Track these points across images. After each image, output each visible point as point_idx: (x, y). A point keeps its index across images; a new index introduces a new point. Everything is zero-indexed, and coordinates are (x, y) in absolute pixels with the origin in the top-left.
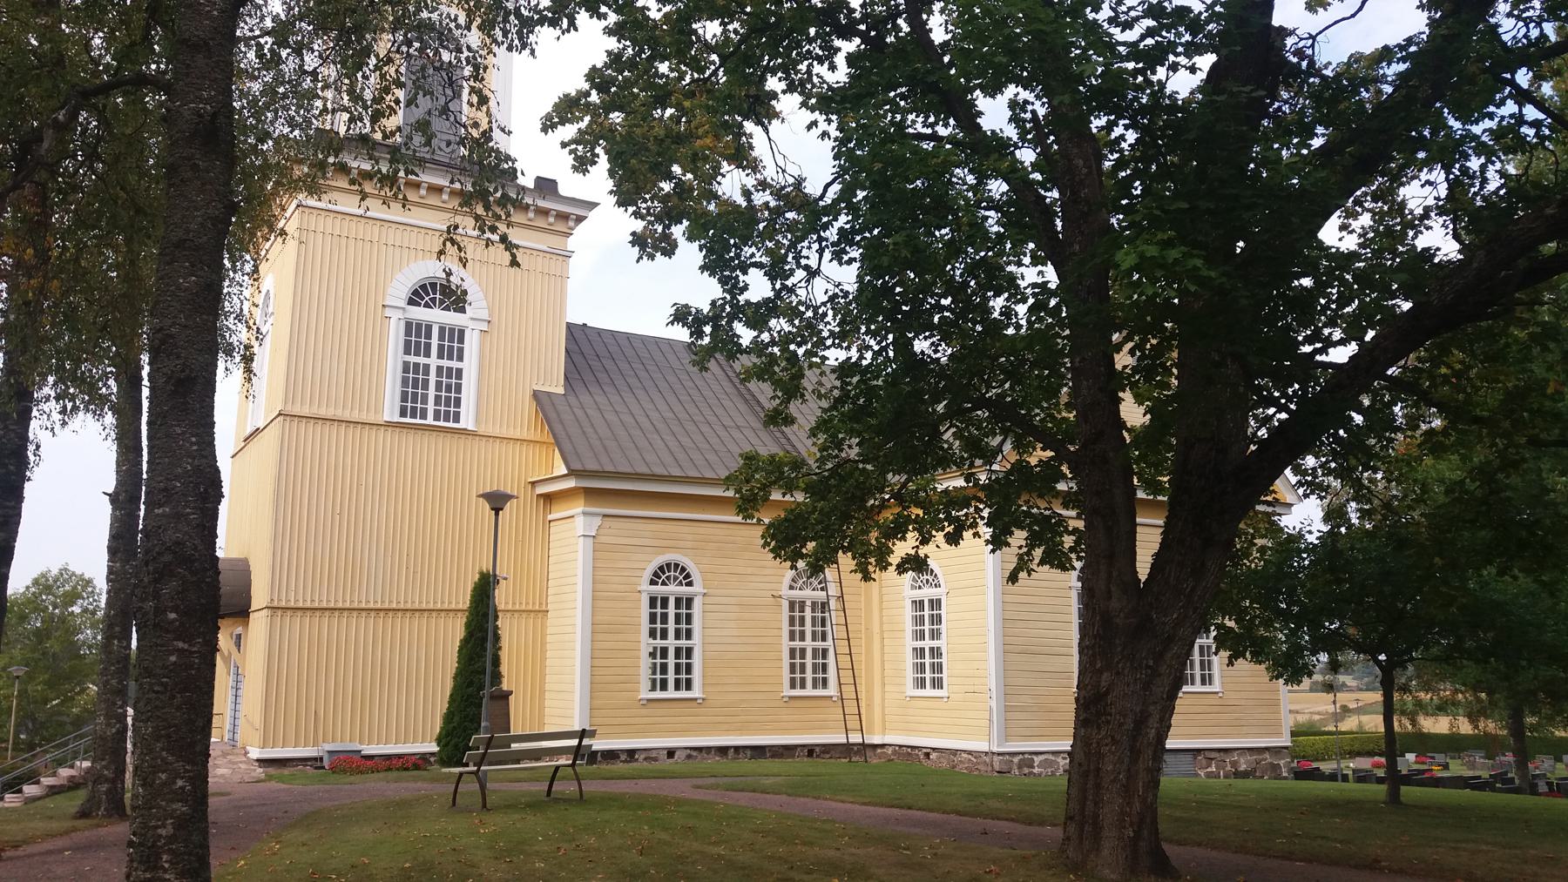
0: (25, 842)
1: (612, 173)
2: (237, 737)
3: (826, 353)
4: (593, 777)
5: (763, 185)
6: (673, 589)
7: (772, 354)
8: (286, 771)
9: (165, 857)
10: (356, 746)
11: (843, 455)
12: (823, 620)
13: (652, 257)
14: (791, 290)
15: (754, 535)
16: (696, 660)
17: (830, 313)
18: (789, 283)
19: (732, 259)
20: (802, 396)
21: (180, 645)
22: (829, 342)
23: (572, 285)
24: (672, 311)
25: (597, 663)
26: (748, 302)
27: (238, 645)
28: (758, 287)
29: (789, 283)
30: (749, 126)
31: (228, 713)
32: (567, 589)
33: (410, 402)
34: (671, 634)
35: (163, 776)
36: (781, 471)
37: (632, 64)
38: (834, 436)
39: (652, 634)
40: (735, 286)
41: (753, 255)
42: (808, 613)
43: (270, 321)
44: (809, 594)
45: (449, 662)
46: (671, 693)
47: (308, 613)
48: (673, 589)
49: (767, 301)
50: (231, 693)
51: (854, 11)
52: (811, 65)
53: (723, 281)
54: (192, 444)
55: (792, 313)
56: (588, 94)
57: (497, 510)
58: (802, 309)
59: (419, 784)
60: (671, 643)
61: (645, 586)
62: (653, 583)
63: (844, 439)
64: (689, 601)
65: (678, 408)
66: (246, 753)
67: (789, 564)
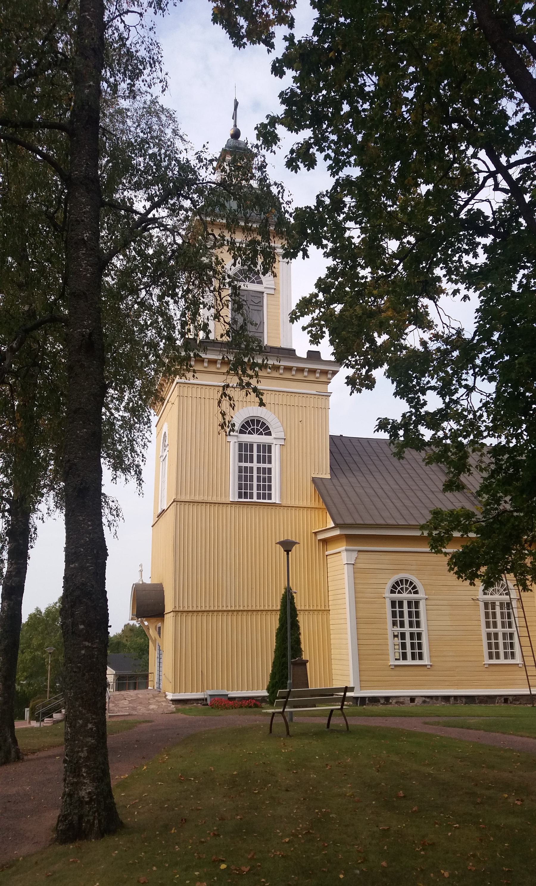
0: (39, 750)
1: (332, 342)
2: (161, 686)
3: (484, 441)
4: (353, 715)
5: (437, 337)
6: (405, 596)
7: (446, 444)
8: (187, 707)
9: (84, 770)
10: (225, 692)
11: (501, 507)
12: (509, 614)
13: (360, 391)
14: (457, 402)
15: (442, 561)
16: (424, 640)
17: (485, 414)
18: (455, 397)
19: (414, 386)
20: (469, 470)
21: (87, 644)
22: (485, 434)
23: (331, 413)
24: (377, 423)
25: (361, 642)
26: (427, 413)
27: (159, 633)
28: (433, 402)
29: (455, 397)
30: (425, 301)
31: (156, 673)
32: (340, 597)
33: (244, 491)
34: (407, 624)
35: (81, 722)
36: (458, 520)
37: (343, 274)
38: (494, 495)
39: (394, 624)
40: (418, 403)
41: (428, 382)
42: (498, 610)
43: (167, 449)
44: (497, 598)
45: (272, 643)
46: (409, 662)
47: (195, 614)
48: (405, 596)
49: (440, 411)
50: (157, 661)
51: (488, 217)
52: (461, 256)
53: (410, 401)
54: (89, 526)
55: (458, 417)
56: (316, 295)
57: (288, 551)
58: (466, 413)
59: (257, 717)
60: (407, 629)
61: (388, 594)
62: (392, 592)
63: (501, 497)
64: (417, 604)
65: (401, 482)
66: (166, 696)
67: (468, 582)
